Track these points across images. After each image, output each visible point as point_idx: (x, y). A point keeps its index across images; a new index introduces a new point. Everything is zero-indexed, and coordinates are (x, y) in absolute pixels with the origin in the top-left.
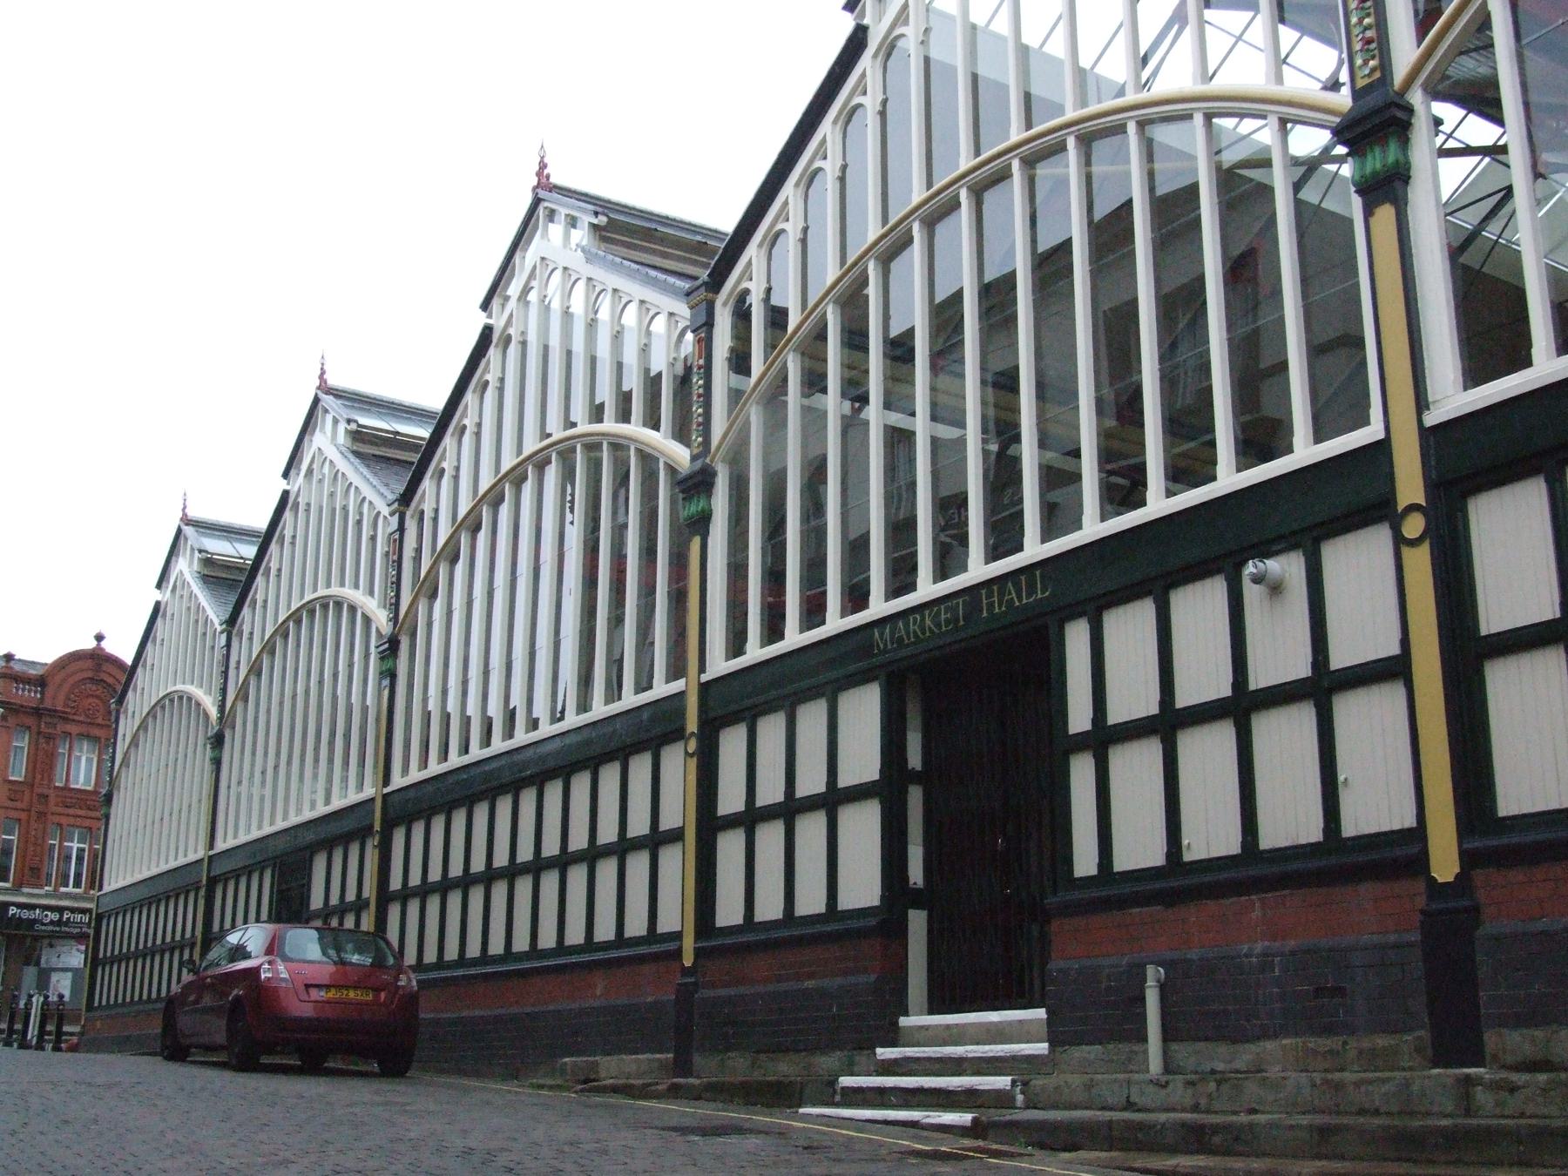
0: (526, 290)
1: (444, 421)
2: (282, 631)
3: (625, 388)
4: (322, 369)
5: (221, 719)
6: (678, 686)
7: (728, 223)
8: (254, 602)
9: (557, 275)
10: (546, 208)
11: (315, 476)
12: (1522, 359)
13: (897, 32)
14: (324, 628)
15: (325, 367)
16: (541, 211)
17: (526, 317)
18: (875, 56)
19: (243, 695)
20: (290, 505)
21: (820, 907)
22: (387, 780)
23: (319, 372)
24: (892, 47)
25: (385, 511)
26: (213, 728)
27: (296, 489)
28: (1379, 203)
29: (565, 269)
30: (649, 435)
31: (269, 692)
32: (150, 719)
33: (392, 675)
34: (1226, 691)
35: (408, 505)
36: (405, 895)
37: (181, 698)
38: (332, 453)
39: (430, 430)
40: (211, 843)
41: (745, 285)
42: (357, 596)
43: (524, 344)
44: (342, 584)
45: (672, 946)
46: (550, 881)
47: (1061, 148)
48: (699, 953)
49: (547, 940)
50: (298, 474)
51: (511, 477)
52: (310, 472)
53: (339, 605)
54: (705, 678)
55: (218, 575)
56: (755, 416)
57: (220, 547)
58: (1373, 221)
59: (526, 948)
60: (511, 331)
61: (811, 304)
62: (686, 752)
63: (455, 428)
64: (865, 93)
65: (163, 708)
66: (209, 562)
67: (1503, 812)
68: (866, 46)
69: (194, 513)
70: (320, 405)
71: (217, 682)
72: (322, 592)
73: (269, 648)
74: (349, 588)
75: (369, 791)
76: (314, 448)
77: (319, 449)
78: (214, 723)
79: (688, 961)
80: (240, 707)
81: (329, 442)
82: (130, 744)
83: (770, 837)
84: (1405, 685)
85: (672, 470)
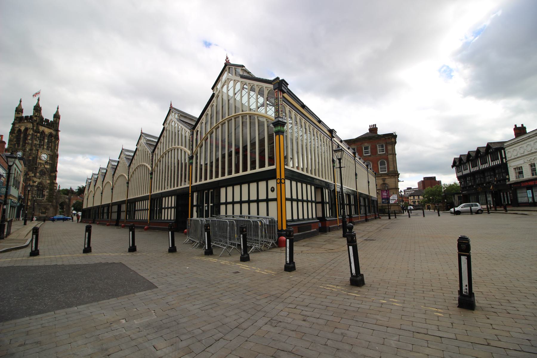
0: (169, 123)
1: (135, 152)
4: (171, 104)
5: (152, 170)
7: (198, 117)
8: (133, 163)
10: (228, 67)
11: (141, 146)
14: (108, 184)
16: (227, 68)
17: (169, 127)
18: (216, 98)
19: (131, 176)
20: (165, 130)
22: (151, 193)
24: (218, 96)
27: (166, 127)
28: (277, 135)
30: (185, 149)
31: (134, 176)
32: (136, 169)
34: (265, 198)
35: (194, 130)
37: (143, 165)
39: (157, 140)
40: (127, 198)
42: (147, 165)
43: (169, 131)
46: (169, 210)
47: (232, 119)
51: (221, 123)
54: (192, 185)
56: (199, 149)
58: (276, 137)
59: (297, 218)
60: (167, 129)
61: (207, 133)
62: (277, 183)
71: (128, 174)
73: (135, 170)
75: (149, 194)
77: (171, 119)
79: (149, 223)
80: (131, 178)
81: (174, 117)
82: (132, 173)
84: (248, 204)
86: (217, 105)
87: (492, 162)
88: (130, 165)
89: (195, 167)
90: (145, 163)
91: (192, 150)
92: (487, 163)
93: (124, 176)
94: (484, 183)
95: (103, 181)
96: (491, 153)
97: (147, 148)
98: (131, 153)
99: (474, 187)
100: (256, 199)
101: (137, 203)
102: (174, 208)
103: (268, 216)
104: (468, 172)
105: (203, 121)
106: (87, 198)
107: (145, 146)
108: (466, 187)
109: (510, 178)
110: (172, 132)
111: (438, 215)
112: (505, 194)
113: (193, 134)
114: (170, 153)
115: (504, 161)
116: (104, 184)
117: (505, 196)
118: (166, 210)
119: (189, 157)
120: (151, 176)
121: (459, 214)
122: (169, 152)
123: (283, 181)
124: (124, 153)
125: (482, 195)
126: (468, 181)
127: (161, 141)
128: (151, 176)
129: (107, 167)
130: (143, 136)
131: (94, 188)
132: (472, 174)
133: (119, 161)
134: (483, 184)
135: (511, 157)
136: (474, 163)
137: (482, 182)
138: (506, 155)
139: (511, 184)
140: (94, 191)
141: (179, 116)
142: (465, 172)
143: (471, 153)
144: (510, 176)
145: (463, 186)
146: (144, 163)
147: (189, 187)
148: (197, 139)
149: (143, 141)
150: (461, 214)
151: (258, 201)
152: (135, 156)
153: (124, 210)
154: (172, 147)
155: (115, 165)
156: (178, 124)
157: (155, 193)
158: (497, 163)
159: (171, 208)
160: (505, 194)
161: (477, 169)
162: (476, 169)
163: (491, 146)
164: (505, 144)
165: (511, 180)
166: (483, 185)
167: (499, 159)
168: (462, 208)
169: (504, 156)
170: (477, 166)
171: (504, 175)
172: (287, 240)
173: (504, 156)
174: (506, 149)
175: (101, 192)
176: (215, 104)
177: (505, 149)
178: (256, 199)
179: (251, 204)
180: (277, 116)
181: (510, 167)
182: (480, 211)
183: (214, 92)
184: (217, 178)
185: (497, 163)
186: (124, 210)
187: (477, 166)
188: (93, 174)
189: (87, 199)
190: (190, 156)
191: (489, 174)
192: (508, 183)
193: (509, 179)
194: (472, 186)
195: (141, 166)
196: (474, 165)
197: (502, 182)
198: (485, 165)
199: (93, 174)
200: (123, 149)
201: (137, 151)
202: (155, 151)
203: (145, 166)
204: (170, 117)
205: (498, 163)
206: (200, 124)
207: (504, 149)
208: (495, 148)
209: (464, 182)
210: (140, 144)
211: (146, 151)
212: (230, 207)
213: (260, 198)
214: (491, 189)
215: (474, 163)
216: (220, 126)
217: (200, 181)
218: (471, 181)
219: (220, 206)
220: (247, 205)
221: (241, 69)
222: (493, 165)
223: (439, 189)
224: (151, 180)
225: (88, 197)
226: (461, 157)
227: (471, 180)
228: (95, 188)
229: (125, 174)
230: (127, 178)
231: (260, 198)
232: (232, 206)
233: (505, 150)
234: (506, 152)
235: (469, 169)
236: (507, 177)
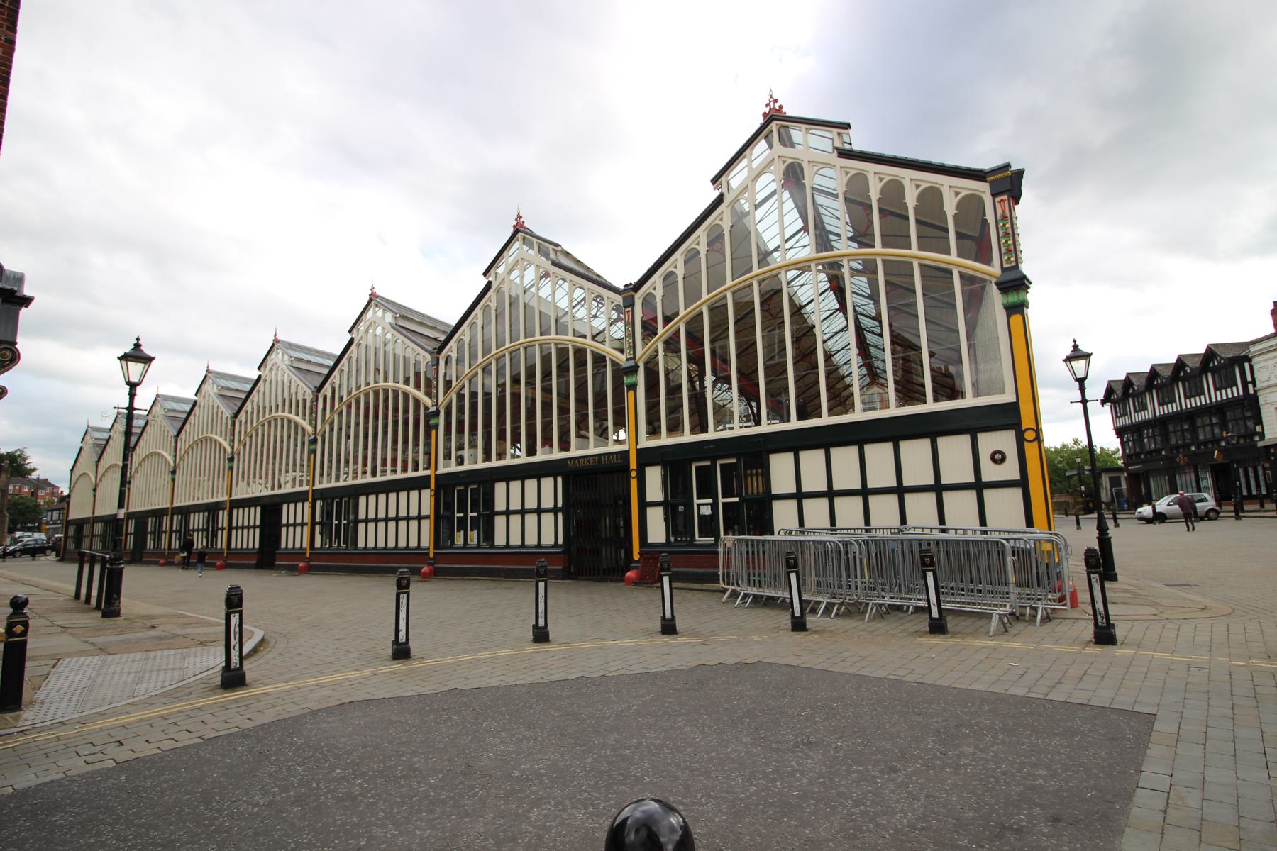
2: (143, 460)
3: (341, 394)
6: (427, 473)
11: (207, 398)
13: (501, 286)
14: (84, 478)
19: (182, 458)
21: (519, 543)
26: (309, 436)
33: (314, 452)
34: (520, 508)
36: (237, 528)
37: (283, 420)
40: (172, 503)
41: (450, 353)
42: (221, 440)
45: (304, 552)
48: (227, 553)
49: (245, 546)
53: (211, 440)
56: (242, 448)
57: (97, 435)
64: (491, 301)
67: (649, 541)
71: (173, 453)
72: (154, 450)
80: (182, 463)
83: (371, 526)
85: (426, 408)
86: (357, 358)
87: (1188, 401)
90: (216, 434)
91: (315, 427)
92: (1204, 394)
93: (162, 456)
94: (1192, 445)
96: (1214, 371)
99: (1164, 453)
100: (536, 507)
102: (218, 529)
103: (986, 526)
104: (1147, 415)
105: (334, 381)
107: (216, 399)
108: (1138, 455)
109: (1266, 432)
111: (1076, 526)
112: (1250, 470)
115: (1251, 391)
116: (101, 470)
117: (1251, 474)
121: (1163, 522)
124: (161, 406)
125: (1185, 473)
126: (1146, 440)
130: (210, 378)
132: (1160, 423)
134: (1189, 446)
135: (1268, 381)
136: (1165, 394)
137: (1188, 441)
138: (1255, 376)
139: (1268, 448)
141: (292, 361)
142: (1139, 417)
143: (1160, 370)
144: (1265, 428)
145: (1132, 452)
148: (240, 432)
149: (210, 388)
150: (1167, 521)
151: (523, 512)
152: (255, 393)
156: (288, 375)
158: (1196, 403)
160: (1250, 470)
161: (1175, 410)
162: (1172, 408)
163: (1218, 351)
164: (1253, 349)
165: (1267, 436)
166: (1140, 457)
167: (1236, 385)
168: (1168, 505)
169: (1249, 379)
170: (1175, 401)
171: (1249, 423)
172: (799, 615)
173: (1249, 379)
174: (1254, 360)
176: (354, 356)
177: (1251, 361)
178: (895, 485)
179: (543, 516)
181: (1266, 404)
182: (1212, 514)
185: (1196, 403)
187: (1127, 415)
191: (1179, 428)
192: (1260, 444)
193: (1262, 435)
194: (1158, 451)
195: (206, 440)
196: (1167, 399)
197: (1154, 454)
198: (1143, 413)
200: (158, 395)
202: (239, 416)
205: (1203, 403)
207: (1249, 359)
208: (1229, 359)
209: (1134, 441)
210: (203, 395)
212: (515, 520)
213: (527, 507)
214: (1215, 460)
215: (1165, 394)
217: (353, 479)
218: (1155, 440)
220: (519, 517)
222: (1189, 406)
223: (1054, 467)
226: (1112, 385)
227: (1154, 436)
229: (166, 451)
231: (512, 508)
233: (1252, 363)
234: (1256, 368)
235: (1154, 409)
236: (1258, 429)
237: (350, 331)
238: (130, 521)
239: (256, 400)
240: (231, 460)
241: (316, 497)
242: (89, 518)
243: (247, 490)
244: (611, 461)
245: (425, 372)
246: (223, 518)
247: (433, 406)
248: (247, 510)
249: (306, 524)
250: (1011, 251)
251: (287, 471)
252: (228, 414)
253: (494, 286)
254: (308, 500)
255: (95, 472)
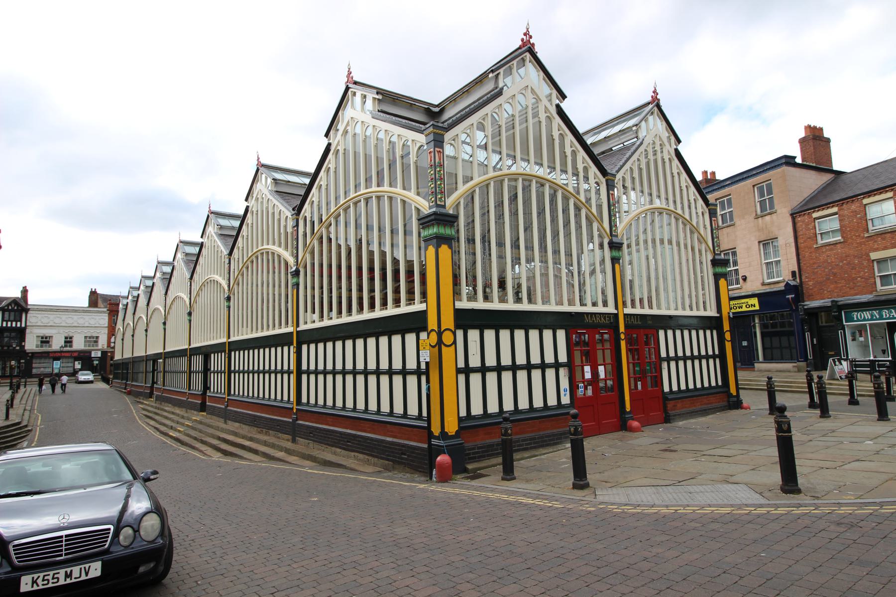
1: (315, 176)
9: (359, 124)
10: (352, 91)
11: (260, 200)
12: (727, 199)
15: (259, 156)
16: (349, 93)
18: (333, 154)
22: (298, 325)
23: (257, 158)
25: (289, 214)
27: (252, 205)
29: (362, 122)
31: (199, 300)
33: (297, 285)
34: (495, 365)
35: (231, 256)
37: (268, 253)
38: (266, 191)
44: (268, 244)
50: (252, 199)
52: (346, 132)
55: (282, 191)
56: (308, 256)
59: (556, 403)
63: (317, 186)
65: (205, 286)
66: (222, 227)
68: (330, 150)
69: (213, 209)
70: (259, 172)
71: (227, 276)
74: (277, 247)
76: (209, 230)
77: (260, 190)
78: (292, 266)
81: (265, 186)
88: (230, 254)
89: (311, 287)
90: (274, 244)
95: (134, 314)
97: (277, 203)
98: (301, 176)
101: (193, 357)
106: (122, 338)
110: (355, 154)
113: (297, 225)
114: (342, 218)
118: (261, 375)
119: (419, 220)
120: (295, 280)
122: (346, 210)
123: (447, 338)
127: (322, 183)
128: (295, 280)
129: (174, 261)
131: (123, 324)
133: (202, 243)
140: (147, 316)
146: (270, 247)
147: (292, 333)
148: (305, 235)
152: (244, 227)
153: (223, 369)
154: (258, 250)
155: (233, 228)
157: (310, 326)
159: (668, 359)
175: (132, 334)
180: (432, 202)
183: (330, 141)
184: (410, 304)
186: (223, 369)
188: (143, 277)
189: (123, 340)
190: (422, 215)
199: (159, 263)
201: (249, 215)
203: (273, 254)
204: (348, 113)
206: (309, 204)
210: (207, 235)
211: (273, 213)
216: (341, 213)
219: (301, 376)
221: (373, 98)
224: (295, 291)
225: (123, 334)
228: (125, 324)
230: (226, 288)
232: (364, 379)
237: (327, 135)
238: (233, 353)
239: (316, 199)
240: (296, 273)
241: (232, 348)
242: (161, 353)
243: (312, 317)
244: (594, 321)
245: (416, 163)
246: (217, 361)
247: (294, 266)
248: (267, 350)
249: (292, 372)
250: (443, 192)
251: (516, 260)
252: (226, 252)
253: (333, 148)
254: (293, 345)
255: (146, 316)
